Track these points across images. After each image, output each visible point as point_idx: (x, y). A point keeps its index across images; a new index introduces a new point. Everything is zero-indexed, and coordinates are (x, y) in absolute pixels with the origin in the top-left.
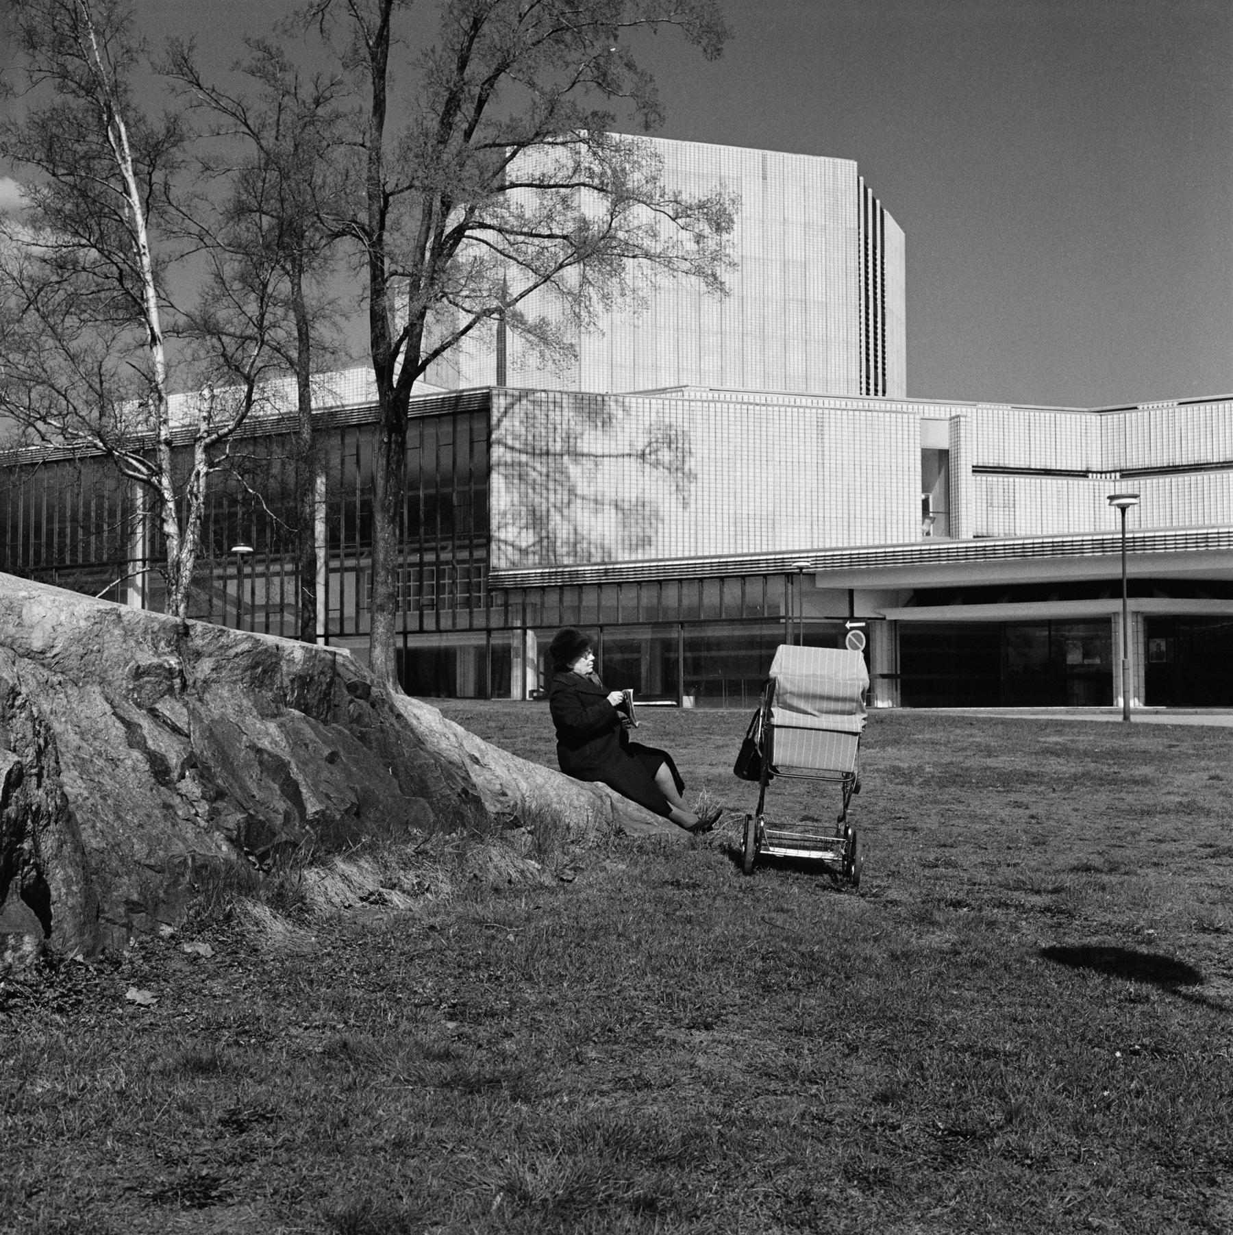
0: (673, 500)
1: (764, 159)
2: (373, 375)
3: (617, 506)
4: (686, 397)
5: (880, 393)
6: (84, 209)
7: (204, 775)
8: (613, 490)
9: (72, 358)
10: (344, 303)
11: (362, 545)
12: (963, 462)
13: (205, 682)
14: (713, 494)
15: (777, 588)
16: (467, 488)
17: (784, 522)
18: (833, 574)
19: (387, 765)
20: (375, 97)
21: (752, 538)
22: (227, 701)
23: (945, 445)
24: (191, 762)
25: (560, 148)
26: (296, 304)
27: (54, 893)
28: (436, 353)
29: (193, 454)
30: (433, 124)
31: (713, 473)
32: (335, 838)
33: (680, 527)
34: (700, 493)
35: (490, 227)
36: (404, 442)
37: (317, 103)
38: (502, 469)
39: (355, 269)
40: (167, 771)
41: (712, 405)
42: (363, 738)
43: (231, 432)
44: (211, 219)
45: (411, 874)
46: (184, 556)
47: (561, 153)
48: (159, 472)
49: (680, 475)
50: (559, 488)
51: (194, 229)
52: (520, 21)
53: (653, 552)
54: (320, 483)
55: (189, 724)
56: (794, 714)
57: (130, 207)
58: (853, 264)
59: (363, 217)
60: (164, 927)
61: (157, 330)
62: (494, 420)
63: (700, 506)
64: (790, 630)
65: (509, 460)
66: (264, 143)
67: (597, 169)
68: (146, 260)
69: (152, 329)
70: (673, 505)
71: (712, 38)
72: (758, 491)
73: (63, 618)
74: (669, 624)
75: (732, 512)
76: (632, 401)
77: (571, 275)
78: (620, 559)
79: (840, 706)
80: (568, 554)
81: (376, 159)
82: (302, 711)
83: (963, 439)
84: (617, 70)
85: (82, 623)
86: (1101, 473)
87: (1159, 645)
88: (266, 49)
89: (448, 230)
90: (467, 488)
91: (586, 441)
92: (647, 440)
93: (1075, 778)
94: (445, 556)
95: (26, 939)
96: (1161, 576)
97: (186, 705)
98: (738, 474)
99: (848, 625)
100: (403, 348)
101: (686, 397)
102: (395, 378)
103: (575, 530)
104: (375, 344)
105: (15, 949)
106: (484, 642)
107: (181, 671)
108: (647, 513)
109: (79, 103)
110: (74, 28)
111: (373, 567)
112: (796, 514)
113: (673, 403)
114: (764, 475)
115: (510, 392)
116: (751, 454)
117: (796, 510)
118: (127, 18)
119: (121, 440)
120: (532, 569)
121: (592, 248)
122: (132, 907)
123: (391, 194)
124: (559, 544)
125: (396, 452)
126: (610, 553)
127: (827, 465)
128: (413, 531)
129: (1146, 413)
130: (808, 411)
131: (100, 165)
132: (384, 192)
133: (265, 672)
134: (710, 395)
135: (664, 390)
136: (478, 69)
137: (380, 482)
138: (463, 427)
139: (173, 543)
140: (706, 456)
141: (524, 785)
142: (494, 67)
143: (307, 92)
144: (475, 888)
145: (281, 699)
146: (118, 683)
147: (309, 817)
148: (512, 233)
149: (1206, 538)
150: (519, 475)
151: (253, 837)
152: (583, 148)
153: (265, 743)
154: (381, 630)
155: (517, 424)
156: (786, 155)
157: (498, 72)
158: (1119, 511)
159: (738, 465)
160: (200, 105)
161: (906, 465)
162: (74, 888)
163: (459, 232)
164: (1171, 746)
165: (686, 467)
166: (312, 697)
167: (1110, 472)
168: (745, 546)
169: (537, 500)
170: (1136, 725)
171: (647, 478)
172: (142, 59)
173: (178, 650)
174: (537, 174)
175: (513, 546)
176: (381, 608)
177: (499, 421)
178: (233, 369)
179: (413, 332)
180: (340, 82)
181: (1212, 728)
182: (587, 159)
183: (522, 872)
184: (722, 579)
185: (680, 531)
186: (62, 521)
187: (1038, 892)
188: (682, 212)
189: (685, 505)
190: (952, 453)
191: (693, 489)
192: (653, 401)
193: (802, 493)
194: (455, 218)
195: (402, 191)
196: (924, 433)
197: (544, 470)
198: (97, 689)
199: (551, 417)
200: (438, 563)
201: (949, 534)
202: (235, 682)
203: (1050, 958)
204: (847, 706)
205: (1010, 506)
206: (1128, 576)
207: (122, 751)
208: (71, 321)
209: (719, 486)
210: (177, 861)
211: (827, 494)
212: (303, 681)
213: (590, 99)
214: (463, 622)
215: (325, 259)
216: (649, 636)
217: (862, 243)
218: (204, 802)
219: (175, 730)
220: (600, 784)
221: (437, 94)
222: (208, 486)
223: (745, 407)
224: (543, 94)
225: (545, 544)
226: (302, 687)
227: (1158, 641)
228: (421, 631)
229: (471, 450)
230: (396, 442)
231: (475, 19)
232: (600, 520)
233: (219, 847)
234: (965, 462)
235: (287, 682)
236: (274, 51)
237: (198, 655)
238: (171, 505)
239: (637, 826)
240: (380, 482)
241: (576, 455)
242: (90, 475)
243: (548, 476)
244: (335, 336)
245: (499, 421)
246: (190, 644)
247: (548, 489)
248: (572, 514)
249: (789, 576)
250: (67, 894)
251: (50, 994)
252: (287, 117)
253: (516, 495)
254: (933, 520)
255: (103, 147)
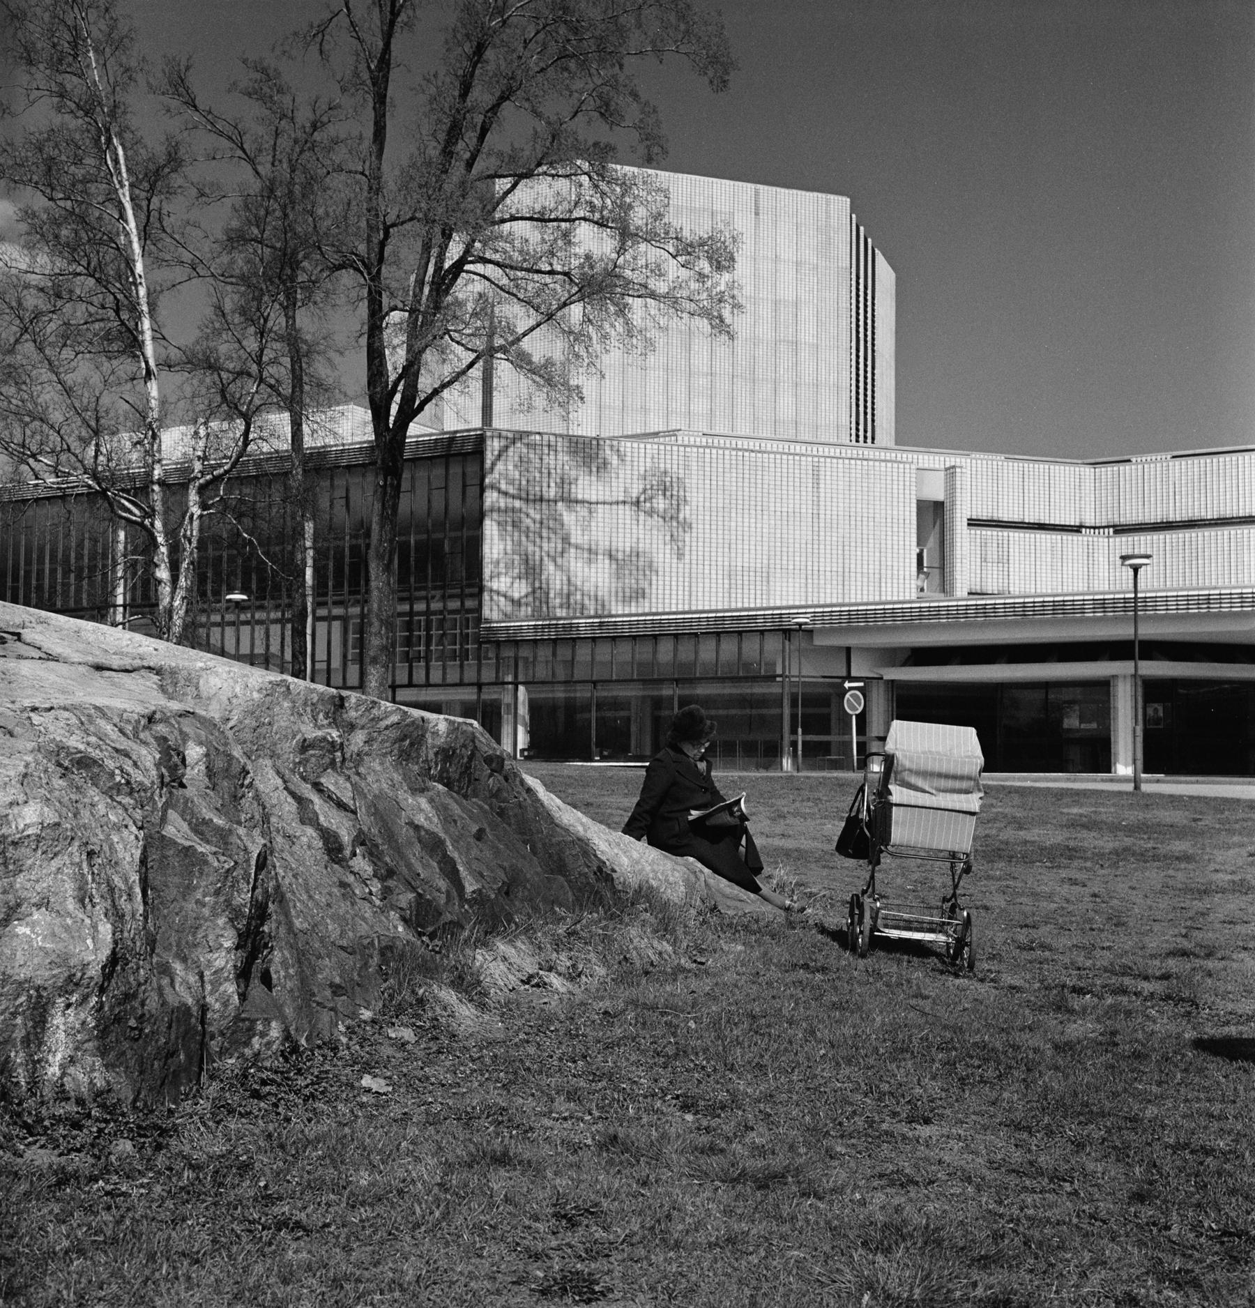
0: (668, 551)
1: (757, 193)
2: (368, 415)
3: (611, 556)
4: (680, 442)
5: (869, 440)
6: (80, 236)
7: (373, 855)
8: (607, 539)
9: (68, 391)
10: (340, 339)
11: (350, 593)
12: (958, 515)
13: (358, 755)
14: (707, 545)
15: (773, 644)
16: (459, 534)
17: (778, 575)
18: (833, 631)
19: (525, 842)
20: (376, 123)
21: (746, 591)
22: (381, 775)
23: (940, 497)
24: (361, 839)
25: (562, 180)
26: (292, 339)
27: (274, 976)
28: (436, 392)
29: (187, 494)
30: (434, 152)
31: (707, 522)
32: (493, 919)
33: (674, 579)
34: (694, 544)
35: (490, 261)
36: (399, 485)
37: (315, 127)
38: (495, 515)
39: (354, 304)
40: (340, 849)
41: (708, 451)
42: (501, 813)
43: (226, 472)
44: (205, 249)
45: (563, 956)
46: (176, 603)
47: (562, 185)
48: (150, 514)
49: (675, 524)
50: (552, 536)
51: (187, 257)
52: (525, 48)
53: (647, 604)
54: (309, 527)
55: (354, 799)
56: (919, 794)
57: (127, 234)
58: (844, 304)
59: (362, 248)
60: (363, 1011)
61: (152, 363)
62: (488, 463)
63: (694, 557)
64: (787, 690)
65: (502, 505)
66: (260, 168)
67: (597, 202)
68: (142, 291)
69: (147, 363)
70: (668, 556)
71: (718, 68)
72: (753, 543)
73: (238, 690)
74: (660, 681)
75: (726, 563)
76: (626, 446)
77: (576, 312)
78: (613, 612)
79: (958, 784)
80: (561, 606)
81: (375, 186)
82: (444, 785)
83: (958, 490)
84: (621, 101)
85: (256, 695)
86: (1095, 528)
87: (1156, 710)
88: (264, 71)
89: (447, 265)
90: (459, 534)
91: (580, 486)
92: (641, 487)
93: (1116, 852)
94: (436, 606)
95: (274, 1024)
96: (1160, 638)
97: (348, 778)
98: (733, 524)
99: (847, 685)
100: (400, 387)
101: (680, 442)
102: (392, 419)
103: (569, 580)
104: (372, 382)
105: (263, 1035)
106: (475, 697)
107: (342, 744)
108: (641, 564)
109: (75, 123)
110: (74, 45)
111: (363, 616)
112: (791, 567)
113: (668, 448)
114: (759, 525)
115: (504, 433)
116: (746, 502)
117: (791, 563)
118: (127, 37)
119: (113, 479)
120: (524, 622)
121: (599, 286)
122: (337, 990)
123: (393, 225)
124: (552, 595)
125: (390, 496)
126: (603, 606)
127: (822, 516)
128: (403, 580)
129: (1140, 467)
130: (803, 458)
131: (97, 190)
132: (384, 223)
133: (412, 744)
134: (704, 440)
135: (656, 434)
136: (481, 96)
137: (375, 527)
138: (456, 470)
139: (166, 589)
140: (701, 504)
141: (625, 861)
142: (498, 94)
143: (304, 116)
144: (628, 972)
145: (426, 773)
146: (286, 756)
147: (468, 896)
148: (512, 268)
149: (1208, 599)
150: (512, 521)
151: (422, 916)
152: (585, 179)
153: (420, 820)
154: (373, 684)
155: (511, 468)
156: (779, 189)
157: (503, 98)
158: (1131, 572)
159: (733, 515)
160: (196, 127)
161: (901, 517)
162: (291, 971)
163: (458, 267)
164: (1195, 820)
165: (681, 516)
166: (454, 771)
167: (1104, 527)
168: (739, 600)
169: (531, 548)
170: (1149, 795)
171: (641, 527)
172: (140, 77)
173: (335, 723)
174: (538, 208)
175: (505, 596)
176: (374, 661)
177: (493, 464)
178: (231, 406)
179: (411, 370)
180: (339, 106)
181: (1226, 801)
182: (588, 193)
183: (660, 953)
184: (718, 634)
185: (674, 583)
186: (41, 560)
187: (1146, 978)
188: (686, 250)
189: (680, 556)
190: (947, 505)
191: (687, 539)
192: (649, 446)
193: (797, 545)
194: (455, 251)
195: (403, 223)
196: (919, 483)
197: (538, 517)
198: (268, 762)
199: (545, 461)
200: (428, 613)
201: (944, 591)
202: (384, 755)
203: (1204, 1049)
204: (964, 785)
205: (1004, 561)
206: (1140, 638)
207: (295, 827)
208: (67, 353)
209: (714, 536)
210: (366, 942)
211: (822, 547)
212: (446, 754)
213: (590, 129)
214: (453, 676)
215: (327, 293)
216: (641, 693)
217: (854, 283)
218: (376, 880)
219: (341, 805)
220: (691, 859)
221: (439, 121)
222: (201, 530)
223: (740, 453)
224: (549, 123)
225: (537, 595)
226: (444, 761)
227: (1156, 705)
228: (410, 685)
229: (464, 493)
230: (392, 485)
231: (479, 44)
232: (593, 570)
233: (396, 927)
234: (962, 512)
235: (431, 756)
236: (271, 73)
237: (352, 727)
238: (163, 549)
239: (729, 903)
240: (375, 527)
241: (571, 502)
242: (79, 514)
243: (541, 523)
244: (329, 371)
245: (493, 464)
246: (345, 716)
247: (541, 537)
248: (566, 564)
249: (787, 633)
250: (285, 977)
251: (301, 1082)
252: (284, 143)
253: (509, 543)
254: (927, 575)
255: (99, 170)
